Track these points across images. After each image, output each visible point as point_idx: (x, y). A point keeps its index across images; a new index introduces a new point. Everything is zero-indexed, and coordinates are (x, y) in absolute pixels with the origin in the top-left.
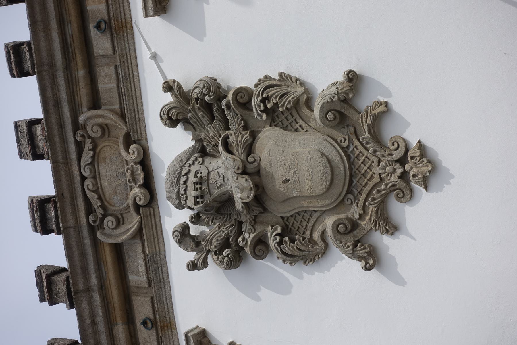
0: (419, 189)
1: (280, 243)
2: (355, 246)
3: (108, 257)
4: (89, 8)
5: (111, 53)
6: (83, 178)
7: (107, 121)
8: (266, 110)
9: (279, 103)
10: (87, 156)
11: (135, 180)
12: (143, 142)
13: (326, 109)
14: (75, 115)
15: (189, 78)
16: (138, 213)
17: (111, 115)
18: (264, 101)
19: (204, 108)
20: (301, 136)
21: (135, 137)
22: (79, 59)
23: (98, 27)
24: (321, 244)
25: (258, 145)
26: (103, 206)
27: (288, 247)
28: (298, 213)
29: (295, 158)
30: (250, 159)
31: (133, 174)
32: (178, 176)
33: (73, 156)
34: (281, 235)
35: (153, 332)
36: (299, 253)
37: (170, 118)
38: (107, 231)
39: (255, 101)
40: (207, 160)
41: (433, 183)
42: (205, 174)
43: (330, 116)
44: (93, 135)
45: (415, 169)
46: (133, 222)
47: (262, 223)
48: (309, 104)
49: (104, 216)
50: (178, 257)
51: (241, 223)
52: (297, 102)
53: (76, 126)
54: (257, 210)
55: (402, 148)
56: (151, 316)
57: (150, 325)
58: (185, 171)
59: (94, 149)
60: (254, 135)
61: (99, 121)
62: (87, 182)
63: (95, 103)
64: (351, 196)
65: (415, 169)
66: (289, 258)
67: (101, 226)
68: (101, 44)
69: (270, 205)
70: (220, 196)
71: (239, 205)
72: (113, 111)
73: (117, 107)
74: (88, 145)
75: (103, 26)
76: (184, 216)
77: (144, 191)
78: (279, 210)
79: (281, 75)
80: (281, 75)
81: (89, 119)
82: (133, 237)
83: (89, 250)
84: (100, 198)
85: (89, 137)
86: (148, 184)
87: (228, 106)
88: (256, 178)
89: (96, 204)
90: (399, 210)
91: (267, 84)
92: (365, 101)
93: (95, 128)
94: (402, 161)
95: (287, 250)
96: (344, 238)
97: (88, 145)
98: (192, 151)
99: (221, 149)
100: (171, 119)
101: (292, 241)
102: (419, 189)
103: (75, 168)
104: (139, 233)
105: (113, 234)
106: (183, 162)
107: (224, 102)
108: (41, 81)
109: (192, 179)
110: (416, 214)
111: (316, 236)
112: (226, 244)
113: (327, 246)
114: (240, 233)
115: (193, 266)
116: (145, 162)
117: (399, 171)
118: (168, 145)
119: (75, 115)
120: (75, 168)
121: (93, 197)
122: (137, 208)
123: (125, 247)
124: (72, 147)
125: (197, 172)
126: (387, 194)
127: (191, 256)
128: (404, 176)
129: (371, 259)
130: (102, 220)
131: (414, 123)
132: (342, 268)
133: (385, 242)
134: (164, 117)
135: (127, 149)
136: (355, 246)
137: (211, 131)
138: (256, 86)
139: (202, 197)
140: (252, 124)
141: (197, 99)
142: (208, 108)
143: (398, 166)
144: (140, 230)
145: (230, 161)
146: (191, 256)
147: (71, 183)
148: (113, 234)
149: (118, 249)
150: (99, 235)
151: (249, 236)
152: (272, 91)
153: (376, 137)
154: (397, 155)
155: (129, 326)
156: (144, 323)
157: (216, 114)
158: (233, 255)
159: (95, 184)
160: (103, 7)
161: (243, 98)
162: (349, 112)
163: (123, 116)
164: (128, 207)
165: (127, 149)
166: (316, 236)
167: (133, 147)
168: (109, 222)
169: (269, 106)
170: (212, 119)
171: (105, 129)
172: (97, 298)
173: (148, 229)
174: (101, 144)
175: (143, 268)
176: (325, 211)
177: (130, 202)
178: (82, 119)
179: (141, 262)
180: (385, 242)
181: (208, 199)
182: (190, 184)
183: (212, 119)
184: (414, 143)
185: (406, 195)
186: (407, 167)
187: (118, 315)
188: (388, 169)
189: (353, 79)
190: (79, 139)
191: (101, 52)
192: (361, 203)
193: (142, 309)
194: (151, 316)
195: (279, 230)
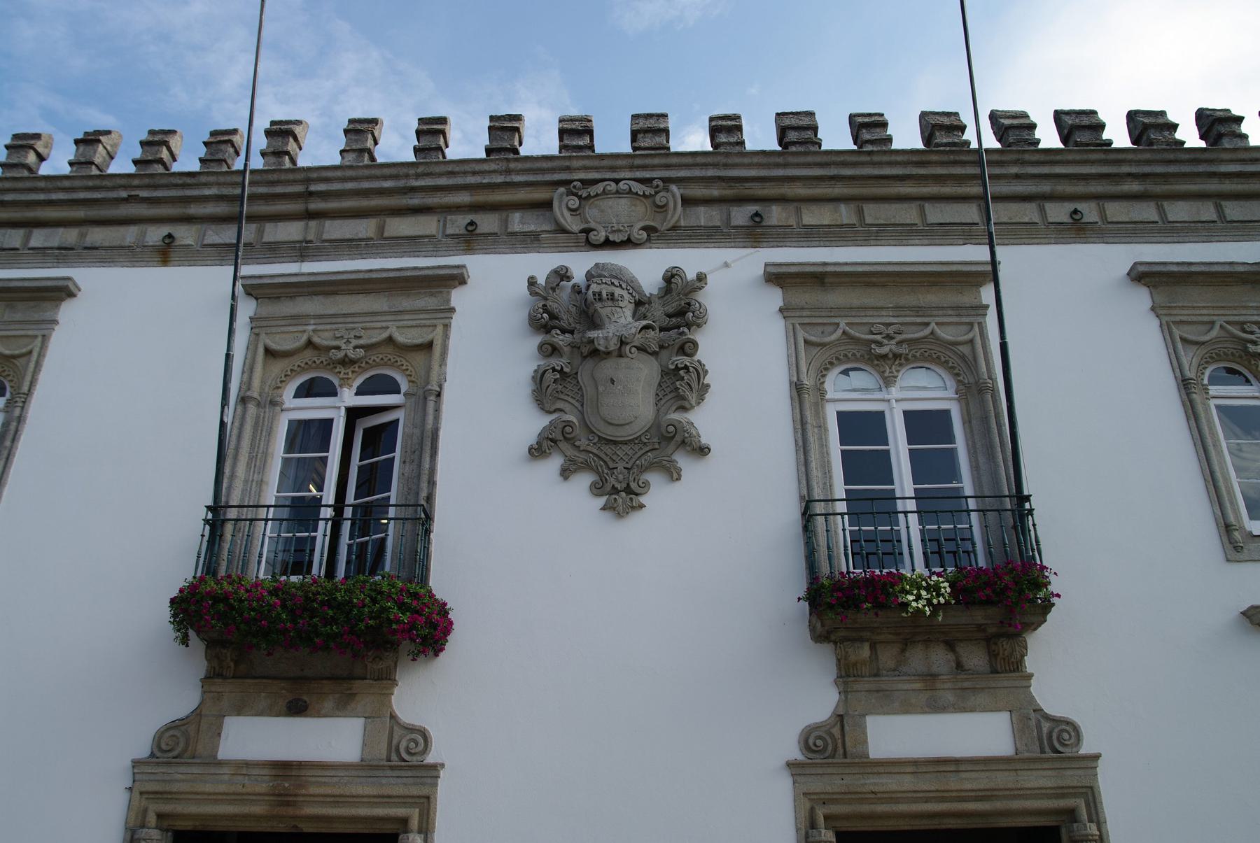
0: (602, 501)
1: (554, 370)
2: (551, 440)
3: (539, 195)
4: (774, 207)
5: (386, 235)
6: (617, 181)
7: (670, 213)
8: (677, 369)
9: (682, 381)
10: (637, 188)
11: (613, 232)
12: (648, 245)
13: (676, 426)
14: (679, 181)
15: (711, 299)
16: (581, 232)
17: (676, 218)
18: (686, 367)
19: (679, 309)
20: (651, 399)
21: (653, 236)
22: (728, 193)
23: (757, 214)
24: (553, 408)
25: (644, 356)
26: (589, 197)
27: (550, 376)
28: (580, 389)
29: (633, 395)
30: (634, 350)
31: (619, 231)
32: (619, 277)
33: (639, 174)
34: (561, 371)
35: (463, 231)
36: (545, 385)
37: (673, 276)
38: (566, 199)
39: (686, 360)
40: (632, 306)
41: (607, 514)
42: (621, 304)
43: (671, 429)
44: (658, 197)
45: (621, 495)
46: (574, 225)
47: (572, 352)
48: (684, 409)
49: (580, 197)
50: (541, 264)
51: (572, 332)
52: (683, 398)
53: (666, 181)
54: (585, 350)
55: (638, 490)
56: (478, 231)
57: (470, 228)
58: (624, 286)
59: (644, 195)
60: (654, 354)
61: (671, 204)
62: (613, 184)
63: (687, 202)
64: (596, 440)
65: (621, 495)
66: (539, 378)
67: (570, 193)
68: (741, 215)
69: (589, 364)
70: (600, 316)
71: (593, 334)
72: (679, 220)
73: (682, 223)
74: (648, 191)
75: (757, 219)
76: (579, 276)
77: (602, 239)
78: (585, 372)
79: (708, 386)
80: (708, 386)
81: (674, 196)
82: (557, 223)
83: (548, 177)
84: (597, 195)
85: (656, 193)
86: (608, 244)
87: (683, 333)
88: (616, 353)
89: (593, 190)
90: (583, 481)
91: (701, 372)
92: (683, 461)
93: (664, 200)
94: (628, 490)
95: (547, 375)
96: (558, 431)
97: (648, 191)
98: (641, 292)
99: (644, 323)
100: (671, 277)
101: (555, 381)
102: (602, 501)
103: (628, 174)
104: (563, 230)
105: (563, 207)
106: (631, 285)
107: (686, 330)
108: (705, 154)
109: (618, 291)
110: (577, 496)
111: (560, 405)
112: (553, 316)
113: (550, 413)
114: (564, 331)
115: (532, 282)
116: (629, 243)
117: (618, 486)
118: (646, 267)
119: (679, 181)
120: (628, 174)
121: (599, 188)
122: (587, 231)
123: (548, 214)
124: (647, 175)
125: (622, 296)
126: (598, 473)
127: (541, 280)
128: (615, 491)
129: (538, 451)
130: (576, 195)
131: (660, 496)
132: (533, 424)
133: (554, 463)
134: (674, 271)
135: (644, 228)
136: (551, 440)
137: (658, 312)
138: (699, 362)
139: (600, 300)
140: (664, 354)
141: (689, 304)
142: (681, 313)
143: (624, 485)
144: (564, 231)
145: (633, 330)
146: (541, 280)
147: (613, 169)
148: (563, 207)
149: (547, 205)
150: (562, 190)
151: (561, 339)
152: (694, 376)
153: (651, 467)
154: (633, 485)
155: (967, 404)
156: (472, 223)
157: (674, 320)
158: (544, 320)
159: (610, 193)
160: (774, 222)
161: (687, 348)
162: (672, 445)
163: (674, 228)
164: (587, 222)
165: (644, 228)
166: (560, 405)
167: (645, 235)
168: (574, 202)
169: (681, 372)
170: (670, 316)
171: (662, 208)
172: (499, 179)
173: (562, 237)
174: (648, 202)
175: (526, 228)
176: (582, 414)
177: (593, 225)
178: (674, 188)
179: (532, 228)
180: (554, 463)
181: (598, 305)
182: (612, 289)
183: (670, 316)
184: (643, 499)
185: (597, 489)
186: (623, 494)
187: (481, 198)
188: (621, 477)
189: (703, 451)
190: (655, 183)
191: (733, 214)
192: (589, 448)
193: (487, 223)
194: (478, 231)
195: (566, 370)
